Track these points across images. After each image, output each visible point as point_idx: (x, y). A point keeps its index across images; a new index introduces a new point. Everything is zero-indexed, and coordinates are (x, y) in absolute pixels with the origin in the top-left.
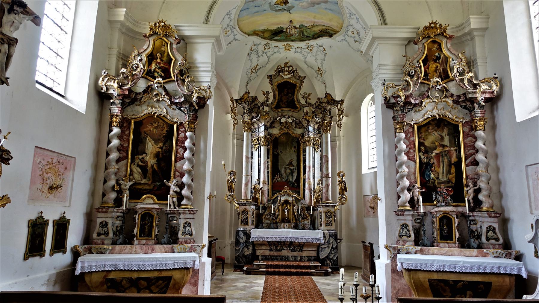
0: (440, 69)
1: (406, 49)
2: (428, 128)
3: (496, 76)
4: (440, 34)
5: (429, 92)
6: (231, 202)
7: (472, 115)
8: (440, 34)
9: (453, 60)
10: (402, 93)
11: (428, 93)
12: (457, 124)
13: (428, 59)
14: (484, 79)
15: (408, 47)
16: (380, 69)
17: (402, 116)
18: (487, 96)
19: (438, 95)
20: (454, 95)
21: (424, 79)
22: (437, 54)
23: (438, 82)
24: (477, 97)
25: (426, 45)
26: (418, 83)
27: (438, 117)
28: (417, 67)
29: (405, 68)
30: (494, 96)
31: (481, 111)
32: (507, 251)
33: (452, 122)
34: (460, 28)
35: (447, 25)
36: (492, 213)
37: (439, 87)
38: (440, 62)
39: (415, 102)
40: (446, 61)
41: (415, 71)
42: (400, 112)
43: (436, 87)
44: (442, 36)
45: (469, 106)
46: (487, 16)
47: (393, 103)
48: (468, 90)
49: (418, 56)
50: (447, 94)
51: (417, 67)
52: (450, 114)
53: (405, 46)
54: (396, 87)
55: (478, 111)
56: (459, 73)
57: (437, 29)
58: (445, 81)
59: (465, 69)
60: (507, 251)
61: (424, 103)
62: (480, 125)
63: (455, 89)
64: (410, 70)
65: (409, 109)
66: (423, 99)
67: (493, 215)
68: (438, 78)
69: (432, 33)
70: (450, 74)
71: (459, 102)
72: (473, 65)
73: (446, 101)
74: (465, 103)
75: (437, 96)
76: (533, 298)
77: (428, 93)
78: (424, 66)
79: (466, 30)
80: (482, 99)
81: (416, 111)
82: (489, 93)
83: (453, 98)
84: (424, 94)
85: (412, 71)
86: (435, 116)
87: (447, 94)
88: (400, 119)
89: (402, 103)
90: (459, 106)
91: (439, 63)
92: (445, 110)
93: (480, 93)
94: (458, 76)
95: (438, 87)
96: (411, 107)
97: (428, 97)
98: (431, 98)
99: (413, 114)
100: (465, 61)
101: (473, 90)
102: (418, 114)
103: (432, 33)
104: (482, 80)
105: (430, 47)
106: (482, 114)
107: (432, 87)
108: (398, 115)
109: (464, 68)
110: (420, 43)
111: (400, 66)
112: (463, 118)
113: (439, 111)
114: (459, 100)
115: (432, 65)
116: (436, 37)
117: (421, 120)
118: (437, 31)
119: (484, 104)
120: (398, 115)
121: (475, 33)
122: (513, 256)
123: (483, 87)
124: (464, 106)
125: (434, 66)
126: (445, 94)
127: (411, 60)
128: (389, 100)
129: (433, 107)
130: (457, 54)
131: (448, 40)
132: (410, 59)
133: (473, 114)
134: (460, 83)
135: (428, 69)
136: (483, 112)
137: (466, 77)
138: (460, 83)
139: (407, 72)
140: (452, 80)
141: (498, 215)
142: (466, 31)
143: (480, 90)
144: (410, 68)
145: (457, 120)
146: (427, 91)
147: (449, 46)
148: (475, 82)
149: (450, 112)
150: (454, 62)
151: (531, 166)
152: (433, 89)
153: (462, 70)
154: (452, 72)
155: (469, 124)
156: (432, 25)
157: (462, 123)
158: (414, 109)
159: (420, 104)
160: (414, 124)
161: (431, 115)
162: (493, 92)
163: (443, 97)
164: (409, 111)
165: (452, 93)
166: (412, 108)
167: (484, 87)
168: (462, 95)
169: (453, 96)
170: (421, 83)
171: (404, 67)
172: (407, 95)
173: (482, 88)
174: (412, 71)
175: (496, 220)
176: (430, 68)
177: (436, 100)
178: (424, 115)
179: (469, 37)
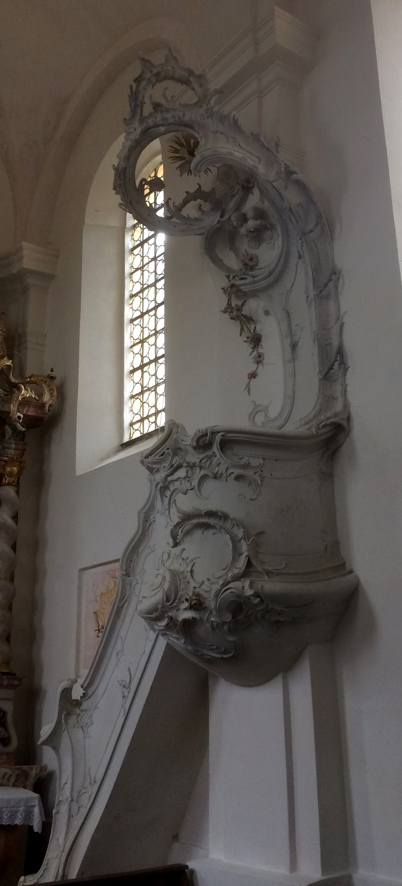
3: (54, 374)
6: (283, 511)
14: (30, 377)
18: (31, 412)
24: (10, 413)
31: (15, 444)
32: (18, 769)
36: (4, 677)
55: (11, 443)
60: (18, 769)
62: (11, 475)
67: (6, 682)
76: (36, 881)
79: (15, 270)
101: (5, 395)
104: (27, 378)
119: (24, 429)
121: (31, 281)
122: (31, 781)
141: (16, 682)
148: (13, 380)
151: (88, 571)
162: (43, 405)
167: (25, 393)
175: (10, 693)
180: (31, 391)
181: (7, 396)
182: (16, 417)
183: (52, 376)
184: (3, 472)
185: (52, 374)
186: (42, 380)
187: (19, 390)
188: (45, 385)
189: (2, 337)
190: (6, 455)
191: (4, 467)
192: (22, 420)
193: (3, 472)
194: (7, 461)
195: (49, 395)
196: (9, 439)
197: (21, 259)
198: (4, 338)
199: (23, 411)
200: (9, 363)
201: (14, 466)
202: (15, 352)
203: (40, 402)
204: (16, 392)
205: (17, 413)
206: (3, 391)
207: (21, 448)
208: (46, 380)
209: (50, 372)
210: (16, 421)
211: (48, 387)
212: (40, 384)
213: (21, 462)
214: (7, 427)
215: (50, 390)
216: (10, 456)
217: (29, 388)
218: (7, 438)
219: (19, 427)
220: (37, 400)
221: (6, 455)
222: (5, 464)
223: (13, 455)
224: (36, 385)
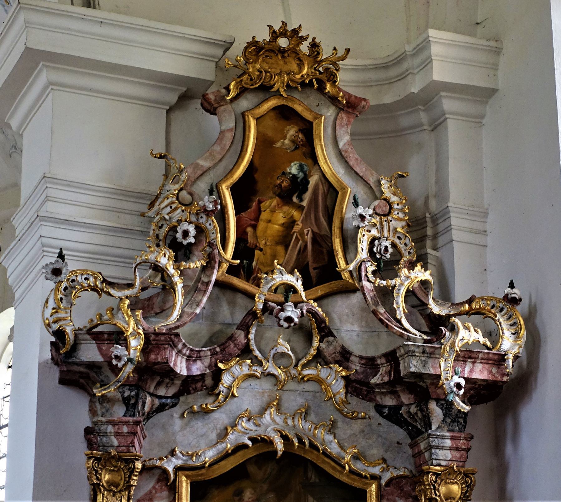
0: (301, 233)
1: (168, 124)
2: (239, 493)
3: (516, 293)
4: (311, 83)
5: (253, 330)
7: (420, 453)
8: (311, 81)
9: (356, 204)
10: (132, 323)
11: (247, 336)
12: (358, 484)
13: (254, 182)
14: (470, 301)
15: (177, 115)
16: (47, 199)
17: (125, 429)
19: (285, 347)
20: (350, 354)
21: (232, 270)
22: (294, 169)
23: (289, 289)
24: (439, 377)
25: (253, 123)
26: (208, 284)
27: (280, 446)
28: (208, 213)
29: (156, 207)
30: (503, 375)
31: (452, 438)
33: (337, 475)
34: (393, 72)
35: (341, 53)
37: (291, 312)
38: (305, 203)
39: (188, 369)
40: (329, 202)
41: (200, 230)
42: (119, 411)
43: (282, 310)
44: (320, 96)
45: (409, 412)
46: (493, 43)
47: (92, 366)
48: (409, 339)
49: (215, 166)
50: (323, 345)
51: (208, 213)
52: (331, 437)
53: (169, 111)
54: (112, 291)
55: (443, 437)
56: (377, 261)
57: (299, 59)
58: (319, 291)
59: (402, 247)
61: (226, 379)
63: (356, 328)
64: (179, 222)
65: (160, 397)
66: (225, 360)
68: (291, 273)
69: (280, 74)
70: (342, 263)
71: (371, 388)
72: (435, 237)
73: (318, 381)
74: (394, 393)
75: (283, 355)
77: (247, 333)
78: (238, 211)
80: (458, 386)
81: (192, 412)
82: (486, 360)
83: (347, 368)
84: (232, 338)
85: (185, 226)
86: (270, 442)
87: (323, 345)
88: (115, 442)
89: (130, 368)
90: (372, 405)
91: (300, 208)
92: (312, 417)
93: (452, 358)
94: (370, 276)
95: (289, 314)
96: (171, 392)
97: (246, 352)
98: (260, 356)
99: (178, 423)
100: (401, 215)
101: (425, 341)
102: (199, 425)
103: (280, 74)
104: (462, 304)
105: (270, 134)
106: (457, 449)
107: (266, 309)
108: (109, 422)
109: (397, 241)
110: (228, 107)
111: (139, 196)
112: (384, 461)
113: (290, 422)
114: (373, 381)
115: (273, 211)
116: (296, 95)
117: (209, 455)
118: (301, 70)
120: (109, 422)
123: (463, 333)
124: (390, 408)
125: (280, 218)
126: (318, 349)
127: (184, 177)
128: (75, 347)
129: (266, 398)
130: (372, 181)
131: (343, 115)
132: (181, 171)
133: (422, 446)
134: (376, 304)
135: (255, 227)
136: (462, 443)
137: (402, 284)
138: (376, 304)
139: (165, 229)
140: (350, 290)
142: (415, 90)
143: (453, 346)
144: (177, 215)
145: (359, 466)
146: (245, 327)
147: (344, 140)
149: (332, 428)
150: (360, 210)
152: (267, 320)
153: (390, 250)
154: (350, 255)
155: (407, 488)
156: (283, 42)
157: (379, 487)
158: (182, 399)
159: (209, 381)
160: (178, 469)
161: (253, 435)
162: (501, 359)
163: (309, 357)
164: (161, 408)
165: (343, 348)
166: (176, 396)
168: (383, 361)
169: (348, 360)
170: (219, 284)
171: (152, 205)
172: (156, 334)
173: (460, 337)
174: (185, 226)
176: (261, 225)
177: (279, 372)
178: (223, 435)
179: (424, 117)
180: (475, 330)
181: (431, 343)
182: (452, 384)
183: (515, 298)
184: (434, 496)
185: (514, 293)
186: (493, 307)
187: (453, 329)
188: (502, 316)
189: (404, 223)
190: (435, 462)
191: (434, 487)
192: (463, 389)
193: (434, 496)
194: (440, 474)
195: (512, 336)
196: (439, 428)
197: (428, 62)
198: (408, 225)
199: (463, 371)
200: (426, 276)
201: (454, 483)
202: (429, 251)
203: (494, 351)
204: (448, 334)
205: (452, 376)
206: (420, 334)
207: (463, 447)
208: (501, 305)
209: (509, 289)
210: (452, 392)
211: (507, 319)
212: (492, 316)
213: (466, 475)
214: (433, 406)
215: (512, 325)
216: (443, 463)
217: (470, 325)
218: (434, 428)
219: (459, 404)
220: (488, 349)
221: (435, 462)
222: (436, 481)
223: (450, 460)
224: (482, 316)
